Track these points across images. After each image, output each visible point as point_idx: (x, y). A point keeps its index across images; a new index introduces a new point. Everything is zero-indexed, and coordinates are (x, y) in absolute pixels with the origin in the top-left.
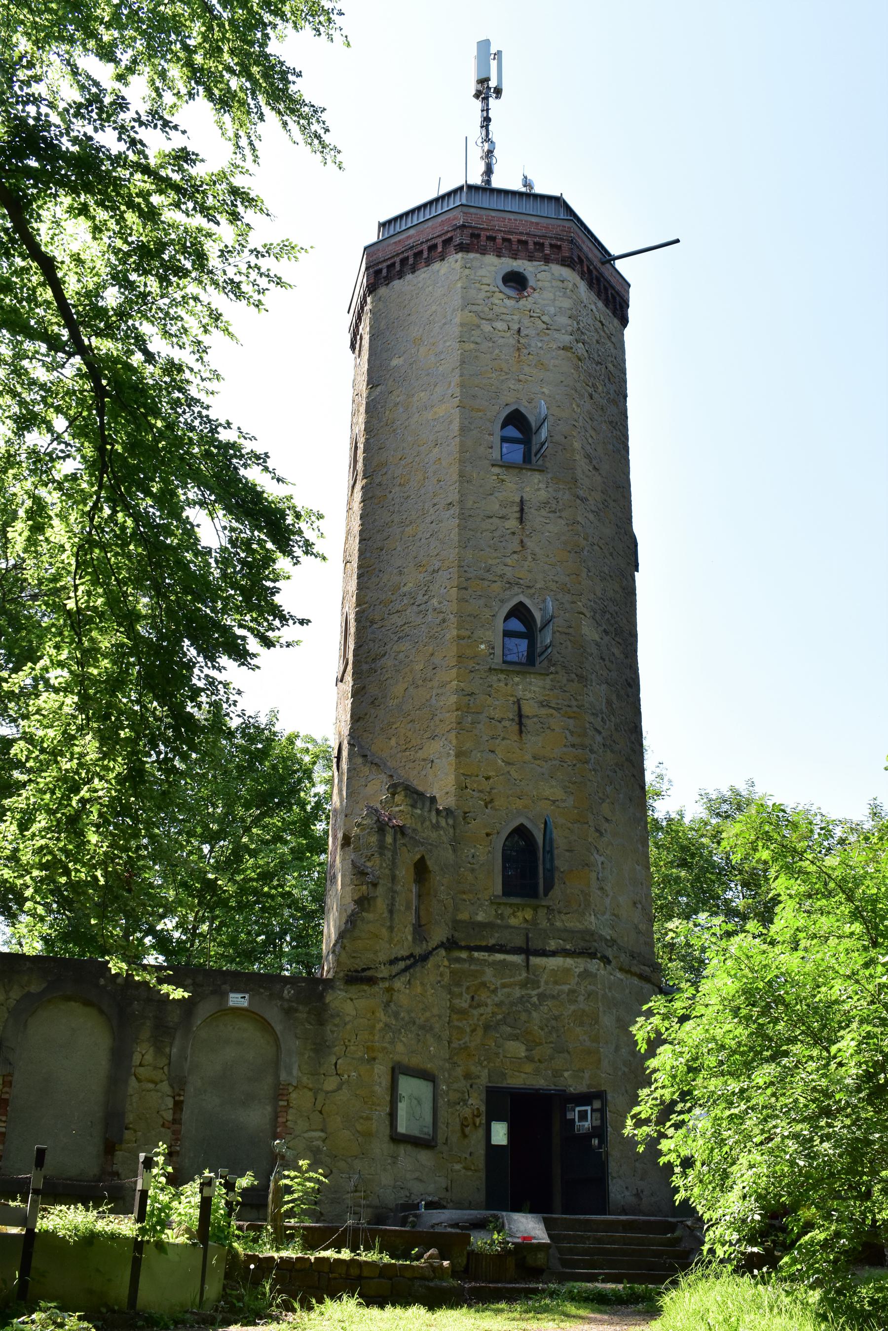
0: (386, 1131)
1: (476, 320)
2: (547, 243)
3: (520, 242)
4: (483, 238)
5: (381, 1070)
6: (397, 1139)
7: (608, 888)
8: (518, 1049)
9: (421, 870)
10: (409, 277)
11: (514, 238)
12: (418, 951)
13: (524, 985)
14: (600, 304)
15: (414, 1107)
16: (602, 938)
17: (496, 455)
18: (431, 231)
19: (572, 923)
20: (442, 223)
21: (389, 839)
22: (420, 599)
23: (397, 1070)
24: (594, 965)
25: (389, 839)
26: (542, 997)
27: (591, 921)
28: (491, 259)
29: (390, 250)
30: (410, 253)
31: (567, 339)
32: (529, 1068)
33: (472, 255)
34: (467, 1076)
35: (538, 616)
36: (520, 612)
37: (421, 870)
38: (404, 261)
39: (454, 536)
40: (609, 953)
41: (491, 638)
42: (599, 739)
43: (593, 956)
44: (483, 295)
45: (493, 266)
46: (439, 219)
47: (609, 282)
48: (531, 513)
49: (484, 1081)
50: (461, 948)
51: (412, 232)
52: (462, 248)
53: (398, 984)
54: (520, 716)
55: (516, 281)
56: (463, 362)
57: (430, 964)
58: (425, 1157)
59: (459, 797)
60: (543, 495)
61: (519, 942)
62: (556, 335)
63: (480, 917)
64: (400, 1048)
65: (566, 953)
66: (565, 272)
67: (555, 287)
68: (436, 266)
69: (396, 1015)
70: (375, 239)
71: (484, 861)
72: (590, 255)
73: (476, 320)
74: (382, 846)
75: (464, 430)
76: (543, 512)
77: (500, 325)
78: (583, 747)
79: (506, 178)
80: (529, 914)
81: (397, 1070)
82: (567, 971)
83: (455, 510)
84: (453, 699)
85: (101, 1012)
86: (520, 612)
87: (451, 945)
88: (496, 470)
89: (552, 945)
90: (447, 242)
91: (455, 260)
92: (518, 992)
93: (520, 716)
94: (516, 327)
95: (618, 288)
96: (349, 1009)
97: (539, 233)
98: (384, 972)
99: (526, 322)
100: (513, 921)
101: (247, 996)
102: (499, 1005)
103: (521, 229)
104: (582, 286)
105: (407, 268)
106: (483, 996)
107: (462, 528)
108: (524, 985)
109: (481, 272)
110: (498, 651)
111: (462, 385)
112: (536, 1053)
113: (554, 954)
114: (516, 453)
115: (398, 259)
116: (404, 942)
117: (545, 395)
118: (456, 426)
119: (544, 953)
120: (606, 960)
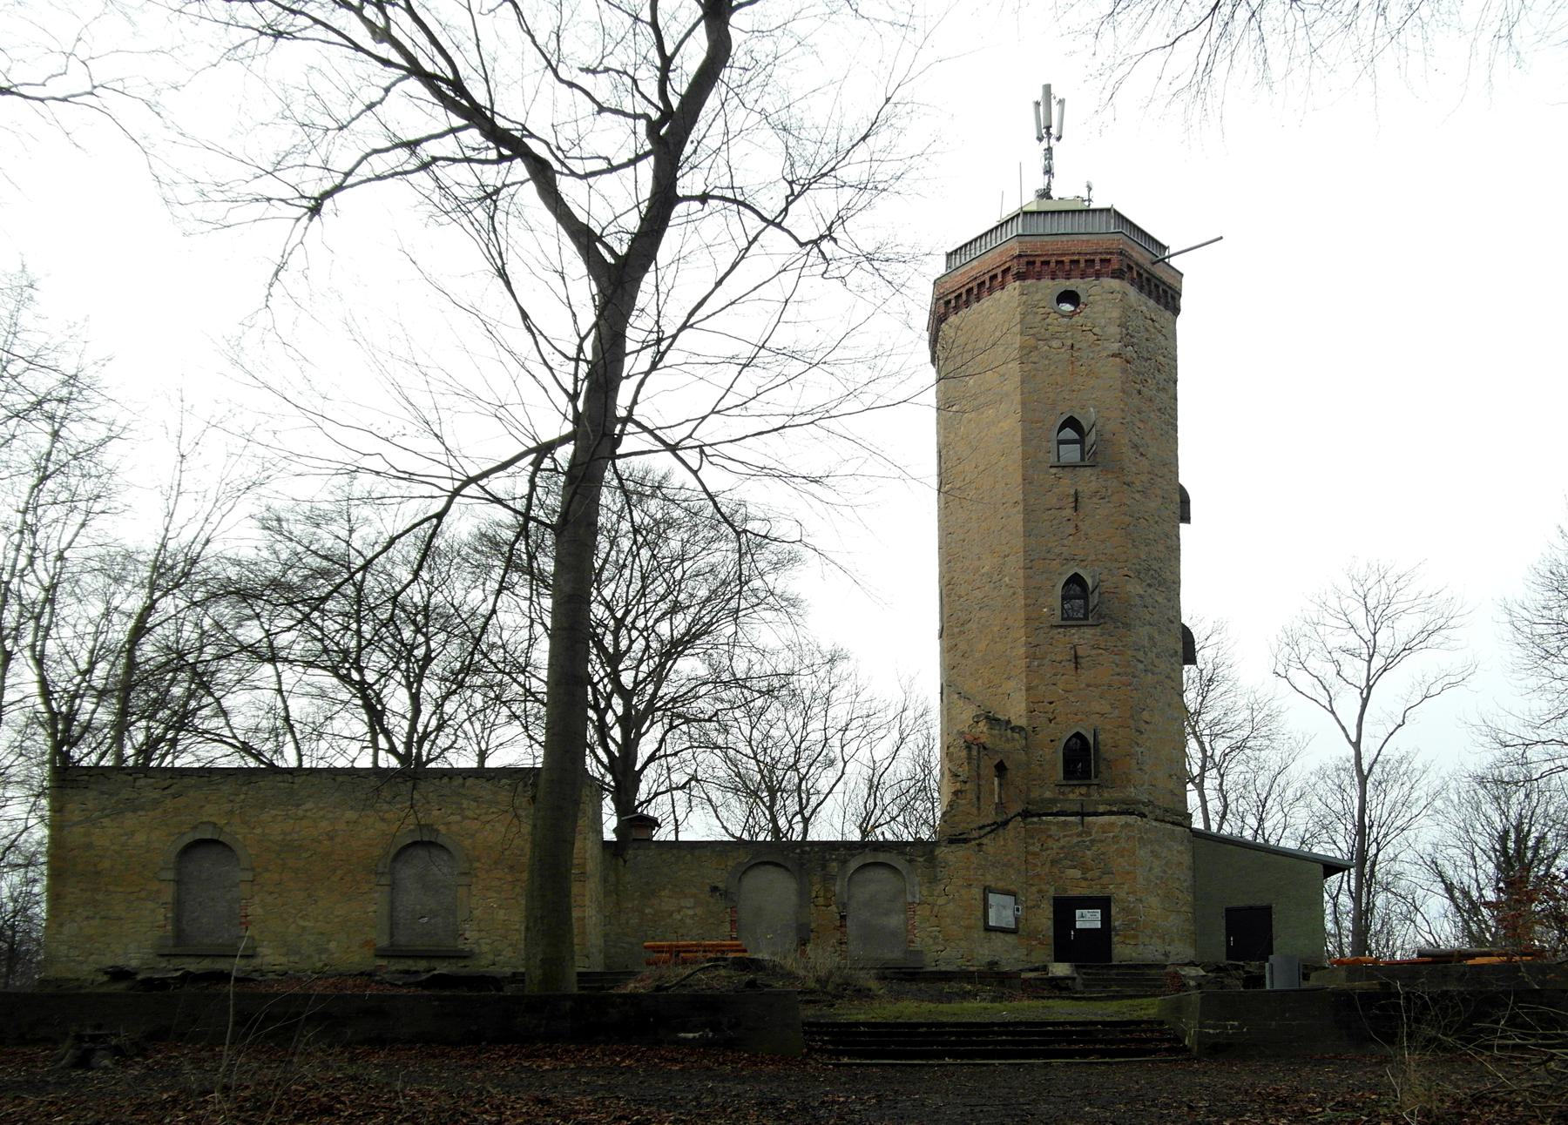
0: (981, 924)
1: (1032, 342)
2: (1097, 258)
3: (1072, 262)
4: (1038, 264)
5: (976, 892)
6: (988, 929)
7: (1146, 768)
8: (1077, 873)
9: (1001, 768)
10: (975, 306)
11: (1066, 259)
12: (999, 820)
13: (1079, 835)
14: (1152, 303)
15: (1002, 912)
16: (1139, 802)
17: (1053, 459)
18: (991, 261)
19: (1116, 794)
20: (1001, 254)
21: (974, 753)
22: (996, 578)
23: (987, 890)
24: (1131, 819)
25: (974, 753)
26: (1092, 841)
27: (1132, 792)
28: (1046, 282)
29: (960, 278)
30: (974, 284)
31: (1116, 346)
32: (1084, 884)
33: (1029, 282)
34: (1039, 891)
35: (1089, 582)
36: (1076, 579)
37: (1001, 768)
38: (969, 291)
39: (1020, 529)
40: (1146, 810)
41: (1053, 599)
42: (1141, 666)
43: (1132, 814)
44: (1039, 317)
45: (1049, 287)
46: (998, 250)
47: (1159, 279)
48: (1084, 501)
49: (1052, 892)
50: (1033, 816)
51: (975, 263)
52: (1020, 276)
53: (985, 841)
54: (1076, 657)
55: (1070, 297)
56: (1023, 382)
57: (1010, 825)
58: (1010, 938)
59: (1029, 718)
60: (1094, 486)
61: (1077, 808)
62: (1106, 344)
63: (1048, 794)
64: (989, 877)
65: (1112, 813)
66: (1115, 284)
67: (1107, 298)
68: (997, 294)
69: (986, 859)
70: (943, 271)
71: (1052, 759)
72: (1141, 261)
73: (1032, 342)
74: (969, 758)
75: (1025, 441)
76: (1095, 500)
77: (1055, 344)
78: (1126, 674)
79: (1066, 189)
80: (1084, 790)
81: (987, 890)
82: (1112, 824)
83: (1020, 507)
84: (1023, 650)
85: (787, 869)
86: (1076, 579)
87: (1026, 814)
88: (1053, 471)
89: (1101, 809)
90: (1005, 272)
91: (1013, 287)
92: (1075, 840)
93: (1076, 657)
94: (1069, 343)
95: (1170, 281)
96: (951, 858)
97: (1089, 250)
98: (975, 834)
99: (1078, 336)
100: (1071, 796)
101: (1078, 912)
102: (1062, 848)
103: (1073, 249)
104: (1132, 292)
105: (973, 297)
106: (1050, 843)
107: (1026, 521)
108: (1079, 835)
109: (1038, 296)
110: (1058, 612)
111: (1023, 404)
112: (1088, 875)
113: (1102, 814)
114: (1071, 453)
115: (964, 290)
116: (990, 816)
117: (1099, 401)
118: (1018, 438)
119: (1096, 814)
120: (1143, 815)
